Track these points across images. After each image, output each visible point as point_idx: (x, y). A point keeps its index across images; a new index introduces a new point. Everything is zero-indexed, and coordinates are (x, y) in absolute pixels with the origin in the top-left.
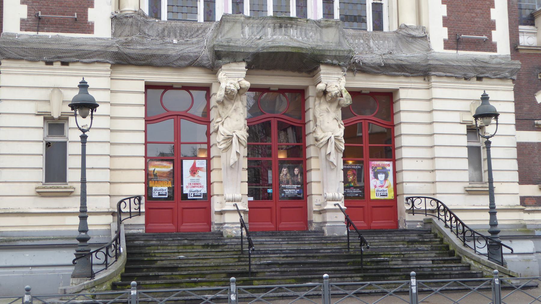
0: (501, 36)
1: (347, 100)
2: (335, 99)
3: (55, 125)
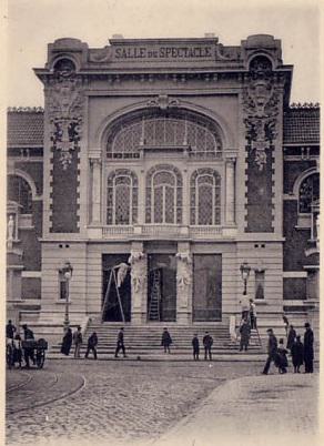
0: (278, 223)
1: (190, 260)
2: (185, 260)
3: (62, 272)
